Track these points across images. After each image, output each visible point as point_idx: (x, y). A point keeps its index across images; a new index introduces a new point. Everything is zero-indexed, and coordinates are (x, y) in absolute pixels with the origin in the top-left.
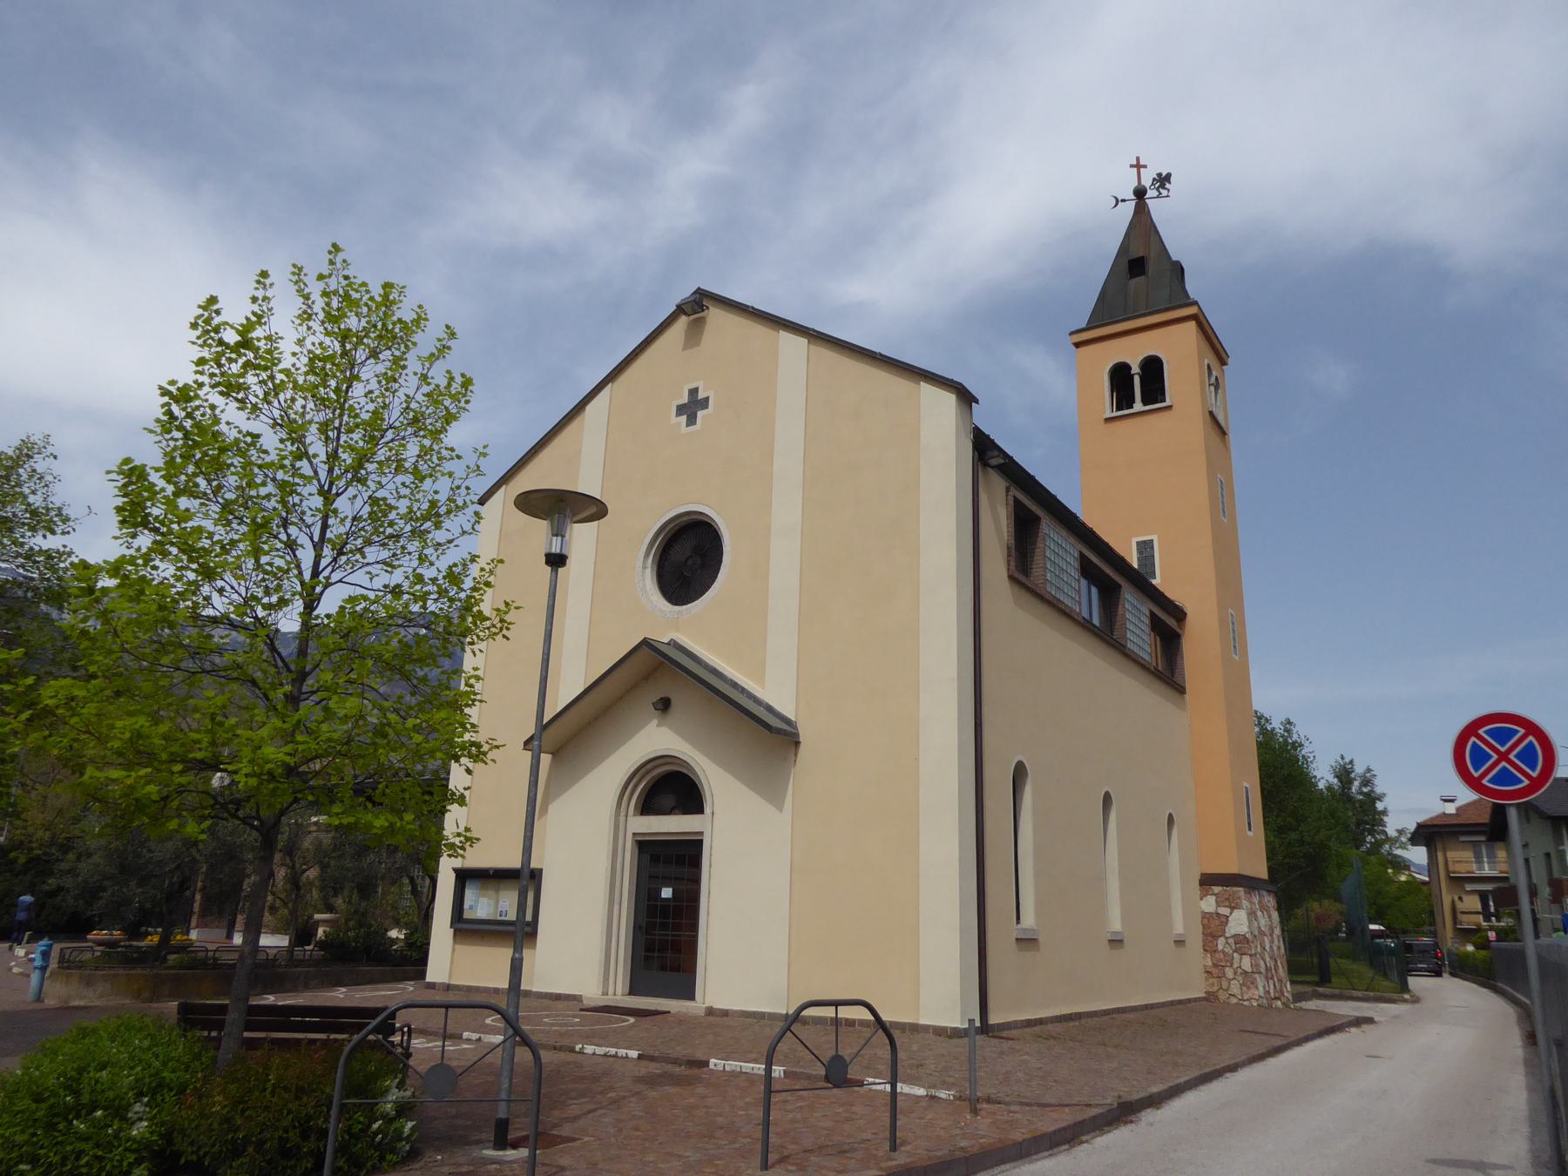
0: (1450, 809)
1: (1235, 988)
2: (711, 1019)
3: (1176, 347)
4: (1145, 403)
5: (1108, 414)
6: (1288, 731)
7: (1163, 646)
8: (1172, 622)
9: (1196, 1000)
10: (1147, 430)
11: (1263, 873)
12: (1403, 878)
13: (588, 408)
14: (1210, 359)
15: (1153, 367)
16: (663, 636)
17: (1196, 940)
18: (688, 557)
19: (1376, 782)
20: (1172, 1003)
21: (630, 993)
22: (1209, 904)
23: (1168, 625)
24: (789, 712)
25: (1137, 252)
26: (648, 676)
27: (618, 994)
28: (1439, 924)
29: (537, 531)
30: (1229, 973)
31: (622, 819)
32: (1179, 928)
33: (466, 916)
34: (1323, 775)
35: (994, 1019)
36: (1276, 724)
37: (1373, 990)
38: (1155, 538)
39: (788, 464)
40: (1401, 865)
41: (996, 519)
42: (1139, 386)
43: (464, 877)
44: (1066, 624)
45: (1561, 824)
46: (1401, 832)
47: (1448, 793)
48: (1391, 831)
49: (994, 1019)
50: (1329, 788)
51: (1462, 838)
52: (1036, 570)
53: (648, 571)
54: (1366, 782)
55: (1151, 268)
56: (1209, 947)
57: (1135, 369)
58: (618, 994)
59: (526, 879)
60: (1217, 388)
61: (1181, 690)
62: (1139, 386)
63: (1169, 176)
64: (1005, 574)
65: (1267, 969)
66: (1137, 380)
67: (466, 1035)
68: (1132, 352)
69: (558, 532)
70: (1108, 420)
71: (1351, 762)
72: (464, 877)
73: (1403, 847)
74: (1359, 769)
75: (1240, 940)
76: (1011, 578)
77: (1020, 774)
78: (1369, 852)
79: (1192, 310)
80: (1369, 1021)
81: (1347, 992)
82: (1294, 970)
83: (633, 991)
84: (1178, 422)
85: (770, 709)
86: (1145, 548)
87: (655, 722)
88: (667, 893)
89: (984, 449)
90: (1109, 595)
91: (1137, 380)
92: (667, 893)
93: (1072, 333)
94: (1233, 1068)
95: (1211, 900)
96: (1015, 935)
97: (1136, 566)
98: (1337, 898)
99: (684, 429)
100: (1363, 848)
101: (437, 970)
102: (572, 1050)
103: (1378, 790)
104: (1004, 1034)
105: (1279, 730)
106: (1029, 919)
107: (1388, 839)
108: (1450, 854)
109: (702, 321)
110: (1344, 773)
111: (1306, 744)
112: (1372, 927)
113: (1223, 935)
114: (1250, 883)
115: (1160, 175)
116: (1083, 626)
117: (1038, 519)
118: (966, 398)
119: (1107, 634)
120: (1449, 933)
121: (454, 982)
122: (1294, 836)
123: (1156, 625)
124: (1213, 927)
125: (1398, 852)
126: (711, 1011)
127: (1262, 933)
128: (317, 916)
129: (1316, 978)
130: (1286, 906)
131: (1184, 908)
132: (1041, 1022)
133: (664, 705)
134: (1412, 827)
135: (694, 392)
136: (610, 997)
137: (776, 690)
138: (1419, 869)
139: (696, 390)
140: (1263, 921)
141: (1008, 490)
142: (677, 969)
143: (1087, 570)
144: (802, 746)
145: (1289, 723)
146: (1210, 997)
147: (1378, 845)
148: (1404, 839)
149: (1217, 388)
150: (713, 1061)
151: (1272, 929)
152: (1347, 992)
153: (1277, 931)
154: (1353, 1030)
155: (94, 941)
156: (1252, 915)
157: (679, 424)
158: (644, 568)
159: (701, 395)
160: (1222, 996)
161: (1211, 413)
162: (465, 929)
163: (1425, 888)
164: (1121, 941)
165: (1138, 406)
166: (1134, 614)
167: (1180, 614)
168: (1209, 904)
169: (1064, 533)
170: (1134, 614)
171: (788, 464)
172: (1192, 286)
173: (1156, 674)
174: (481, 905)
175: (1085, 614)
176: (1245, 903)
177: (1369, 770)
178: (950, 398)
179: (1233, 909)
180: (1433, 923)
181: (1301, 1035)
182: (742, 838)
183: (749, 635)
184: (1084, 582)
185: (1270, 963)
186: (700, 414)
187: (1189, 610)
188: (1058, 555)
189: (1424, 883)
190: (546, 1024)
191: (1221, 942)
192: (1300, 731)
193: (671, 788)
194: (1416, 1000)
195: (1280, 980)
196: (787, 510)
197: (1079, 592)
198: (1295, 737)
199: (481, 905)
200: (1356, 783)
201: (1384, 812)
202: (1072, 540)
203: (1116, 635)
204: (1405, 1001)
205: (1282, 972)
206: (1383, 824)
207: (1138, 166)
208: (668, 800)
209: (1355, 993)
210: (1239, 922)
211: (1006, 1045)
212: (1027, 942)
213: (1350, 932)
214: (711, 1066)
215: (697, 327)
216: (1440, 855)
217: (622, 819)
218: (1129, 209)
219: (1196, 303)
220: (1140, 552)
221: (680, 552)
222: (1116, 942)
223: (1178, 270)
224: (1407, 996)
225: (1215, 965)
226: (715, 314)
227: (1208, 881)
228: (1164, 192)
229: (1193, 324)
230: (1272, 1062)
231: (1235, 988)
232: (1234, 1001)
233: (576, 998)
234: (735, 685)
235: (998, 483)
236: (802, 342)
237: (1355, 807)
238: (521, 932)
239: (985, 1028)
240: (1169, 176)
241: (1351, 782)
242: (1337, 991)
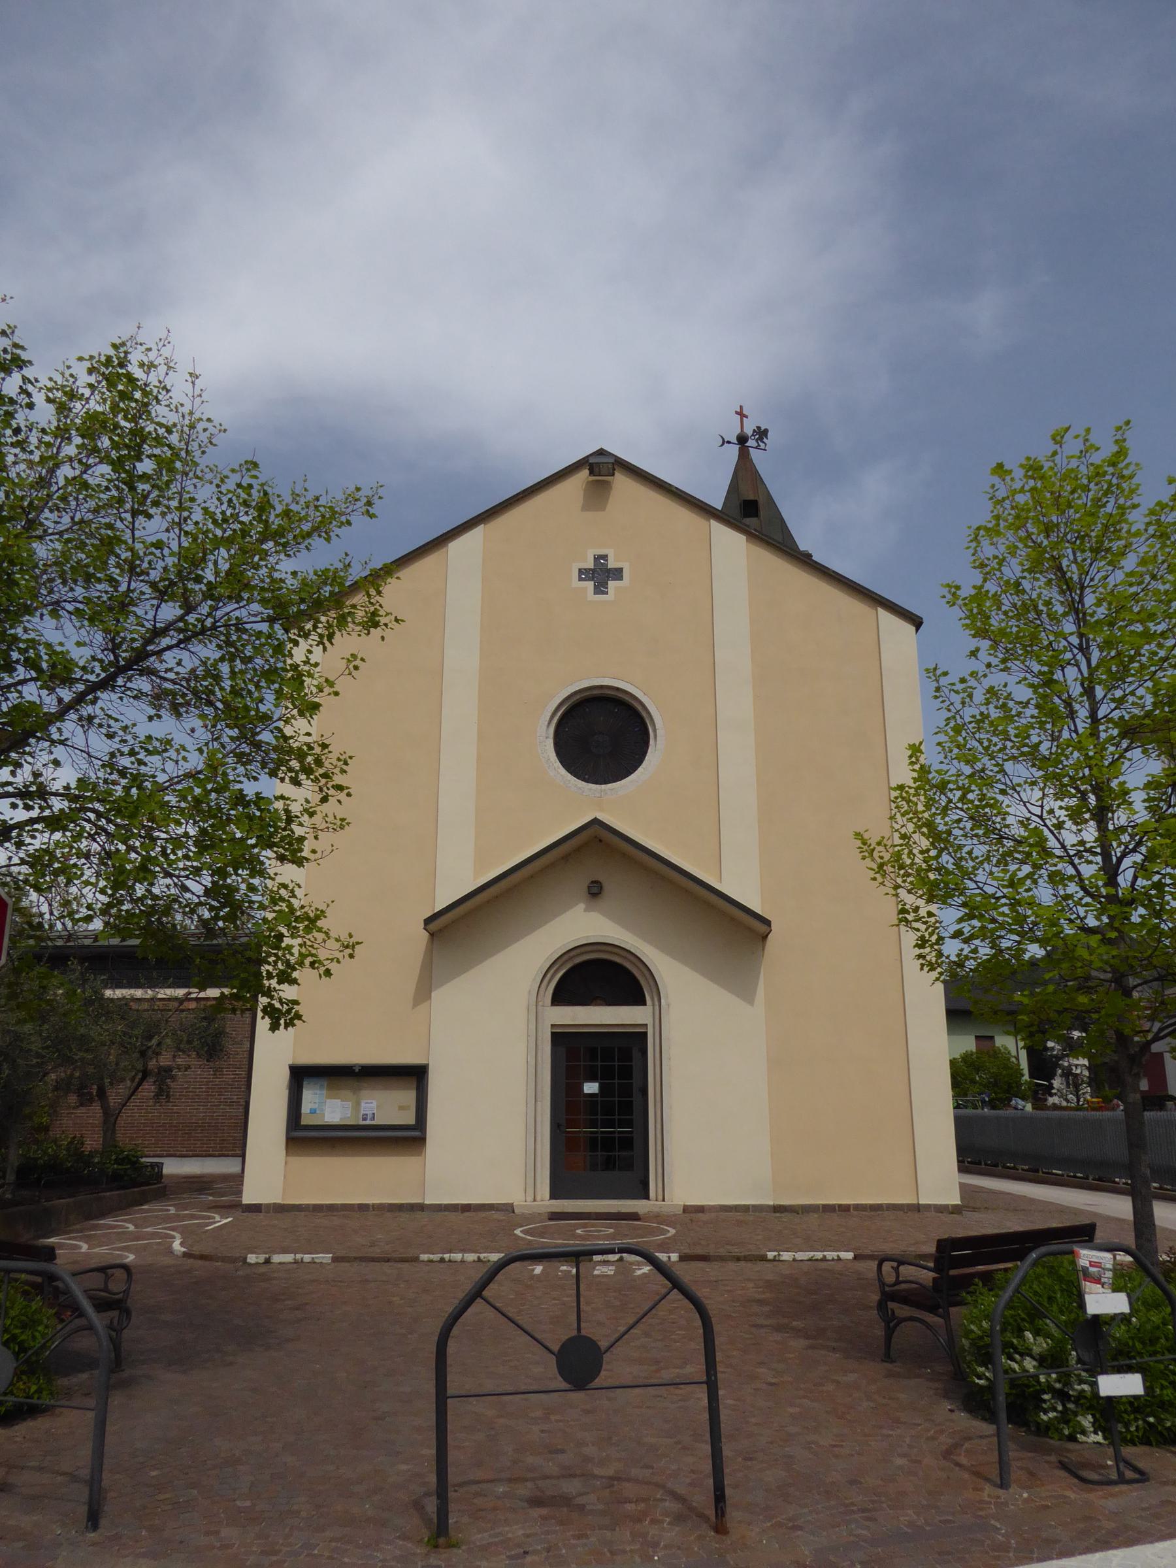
18: (602, 733)
43: (300, 1075)
45: (1167, 976)
58: (544, 1202)
63: (766, 431)
72: (300, 1075)
83: (553, 1196)
88: (591, 1088)
102: (763, 1258)
115: (759, 428)
133: (595, 891)
137: (741, 883)
139: (605, 557)
142: (629, 1166)
162: (303, 1137)
196: (736, 702)
199: (328, 1108)
207: (741, 414)
226: (621, 482)
240: (766, 431)
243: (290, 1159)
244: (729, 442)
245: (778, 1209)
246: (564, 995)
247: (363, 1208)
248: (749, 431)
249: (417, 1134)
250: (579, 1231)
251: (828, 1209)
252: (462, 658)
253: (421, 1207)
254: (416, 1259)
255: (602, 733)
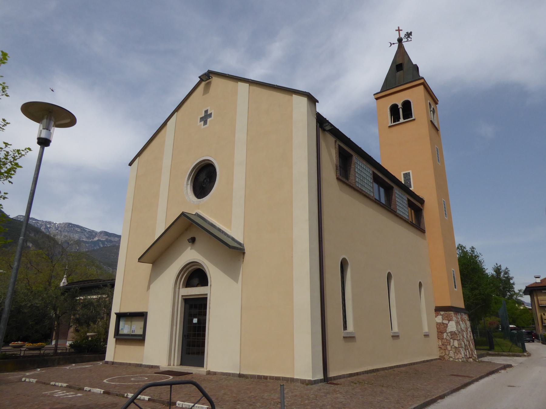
0: (538, 280)
1: (452, 354)
2: (208, 376)
3: (415, 96)
4: (404, 119)
5: (390, 124)
6: (473, 251)
7: (415, 214)
8: (419, 204)
9: (435, 360)
10: (406, 129)
11: (462, 305)
12: (522, 308)
13: (168, 123)
14: (430, 100)
15: (407, 105)
16: (191, 211)
17: (434, 334)
18: (204, 178)
19: (510, 273)
20: (424, 362)
21: (181, 365)
22: (439, 319)
23: (416, 205)
24: (240, 240)
25: (399, 62)
26: (187, 229)
27: (176, 367)
28: (536, 322)
29: (33, 129)
30: (449, 347)
31: (177, 289)
32: (426, 330)
33: (121, 332)
34: (490, 270)
35: (331, 374)
36: (468, 249)
37: (511, 352)
38: (410, 171)
39: (241, 136)
40: (521, 303)
41: (330, 155)
42: (401, 113)
43: (120, 316)
44: (365, 200)
46: (520, 291)
47: (537, 275)
48: (516, 291)
49: (331, 374)
50: (493, 276)
51: (543, 292)
52: (352, 177)
53: (189, 186)
54: (506, 273)
55: (405, 67)
56: (440, 337)
57: (400, 106)
59: (142, 316)
60: (434, 113)
61: (423, 231)
62: (401, 113)
64: (335, 177)
65: (465, 345)
66: (401, 110)
67: (85, 388)
68: (398, 99)
69: (47, 128)
70: (390, 127)
71: (500, 266)
73: (521, 296)
74: (503, 268)
75: (453, 334)
76: (338, 179)
77: (344, 265)
78: (508, 299)
79: (422, 81)
80: (510, 366)
81: (500, 353)
82: (477, 344)
84: (417, 127)
85: (233, 239)
86: (407, 176)
87: (190, 248)
89: (321, 122)
90: (389, 191)
91: (401, 110)
92: (195, 321)
93: (374, 95)
94: (442, 397)
95: (440, 317)
96: (343, 335)
97: (403, 182)
98: (497, 315)
99: (203, 127)
100: (506, 297)
101: (109, 356)
102: (123, 396)
103: (511, 276)
104: (335, 382)
105: (469, 251)
106: (351, 328)
107: (515, 294)
108: (539, 298)
109: (210, 83)
110: (498, 270)
111: (480, 256)
112: (511, 326)
113: (446, 332)
114: (456, 310)
115: (407, 33)
116: (375, 202)
117: (352, 156)
118: (313, 100)
119: (388, 207)
120: (541, 328)
121: (116, 361)
122: (477, 292)
123: (411, 205)
124: (441, 329)
125: (519, 298)
126: (209, 373)
127: (462, 331)
128: (88, 334)
129: (488, 347)
130: (474, 320)
131: (428, 321)
132: (357, 374)
133: (193, 240)
134: (524, 288)
135: (206, 111)
136: (172, 366)
137: (235, 231)
138: (528, 304)
140: (463, 326)
141: (336, 142)
142: (198, 353)
143: (376, 179)
144: (246, 255)
145: (473, 248)
146: (441, 358)
147: (511, 296)
148: (521, 293)
149: (434, 113)
150: (178, 402)
151: (467, 329)
152: (500, 353)
153: (469, 329)
154: (503, 371)
155: (12, 346)
156: (457, 323)
157: (201, 125)
158: (187, 184)
159: (209, 113)
160: (447, 358)
161: (431, 121)
162: (121, 338)
163: (530, 311)
164: (398, 336)
165: (402, 120)
166: (400, 200)
167: (422, 201)
168: (439, 319)
169: (364, 163)
170: (400, 200)
171: (241, 136)
172: (421, 74)
173: (411, 224)
174: (126, 328)
175: (377, 198)
176: (454, 318)
177: (507, 269)
178: (304, 100)
179: (449, 321)
180: (534, 324)
181: (478, 377)
182: (223, 295)
183: (227, 211)
184: (376, 186)
185: (467, 343)
186: (208, 120)
187: (425, 199)
188: (361, 172)
189: (530, 309)
190: (131, 381)
191: (445, 334)
192: (477, 251)
193: (196, 276)
194: (529, 355)
195: (472, 350)
196: (240, 154)
197: (373, 188)
198: (476, 253)
199: (126, 328)
200: (502, 274)
201: (513, 284)
202: (369, 166)
203: (392, 207)
204: (525, 356)
205: (472, 346)
206: (513, 288)
207: (399, 30)
208: (196, 281)
209: (504, 353)
210: (452, 326)
211: (333, 387)
212: (350, 338)
213: (503, 328)
214: (177, 405)
215: (208, 85)
216: (535, 298)
217: (177, 289)
218: (395, 47)
219: (423, 78)
220: (405, 178)
221: (203, 177)
222: (396, 337)
223: (416, 68)
224: (525, 354)
225: (443, 345)
226: (215, 80)
227: (438, 309)
228: (409, 39)
229: (422, 87)
230: (463, 391)
231: (452, 354)
232: (451, 359)
233: (158, 367)
234: (220, 230)
235: (331, 139)
236: (247, 85)
237: (502, 282)
238: (139, 339)
239: (326, 379)
240: (411, 33)
241: (500, 273)
242: (497, 353)
243: (117, 346)
244: (394, 44)
245: (240, 376)
246: (188, 284)
247: (130, 364)
248: (402, 35)
249: (141, 338)
250: (132, 379)
251: (259, 377)
252: (167, 162)
253: (140, 366)
254: (49, 384)
255: (204, 178)
